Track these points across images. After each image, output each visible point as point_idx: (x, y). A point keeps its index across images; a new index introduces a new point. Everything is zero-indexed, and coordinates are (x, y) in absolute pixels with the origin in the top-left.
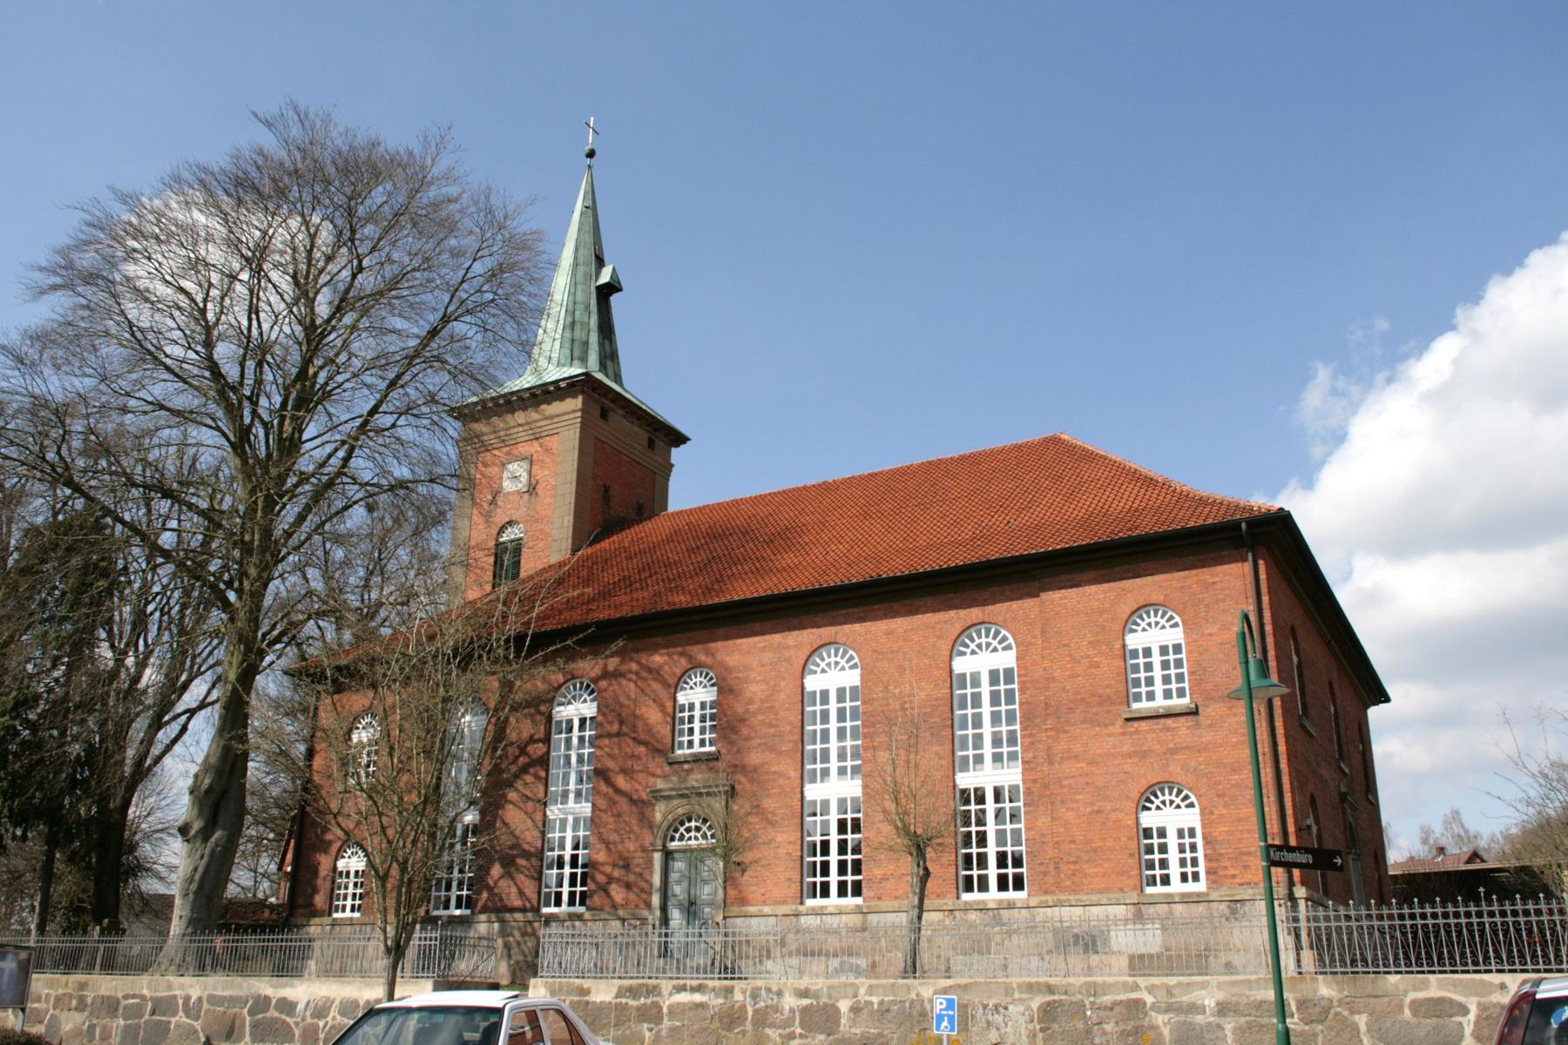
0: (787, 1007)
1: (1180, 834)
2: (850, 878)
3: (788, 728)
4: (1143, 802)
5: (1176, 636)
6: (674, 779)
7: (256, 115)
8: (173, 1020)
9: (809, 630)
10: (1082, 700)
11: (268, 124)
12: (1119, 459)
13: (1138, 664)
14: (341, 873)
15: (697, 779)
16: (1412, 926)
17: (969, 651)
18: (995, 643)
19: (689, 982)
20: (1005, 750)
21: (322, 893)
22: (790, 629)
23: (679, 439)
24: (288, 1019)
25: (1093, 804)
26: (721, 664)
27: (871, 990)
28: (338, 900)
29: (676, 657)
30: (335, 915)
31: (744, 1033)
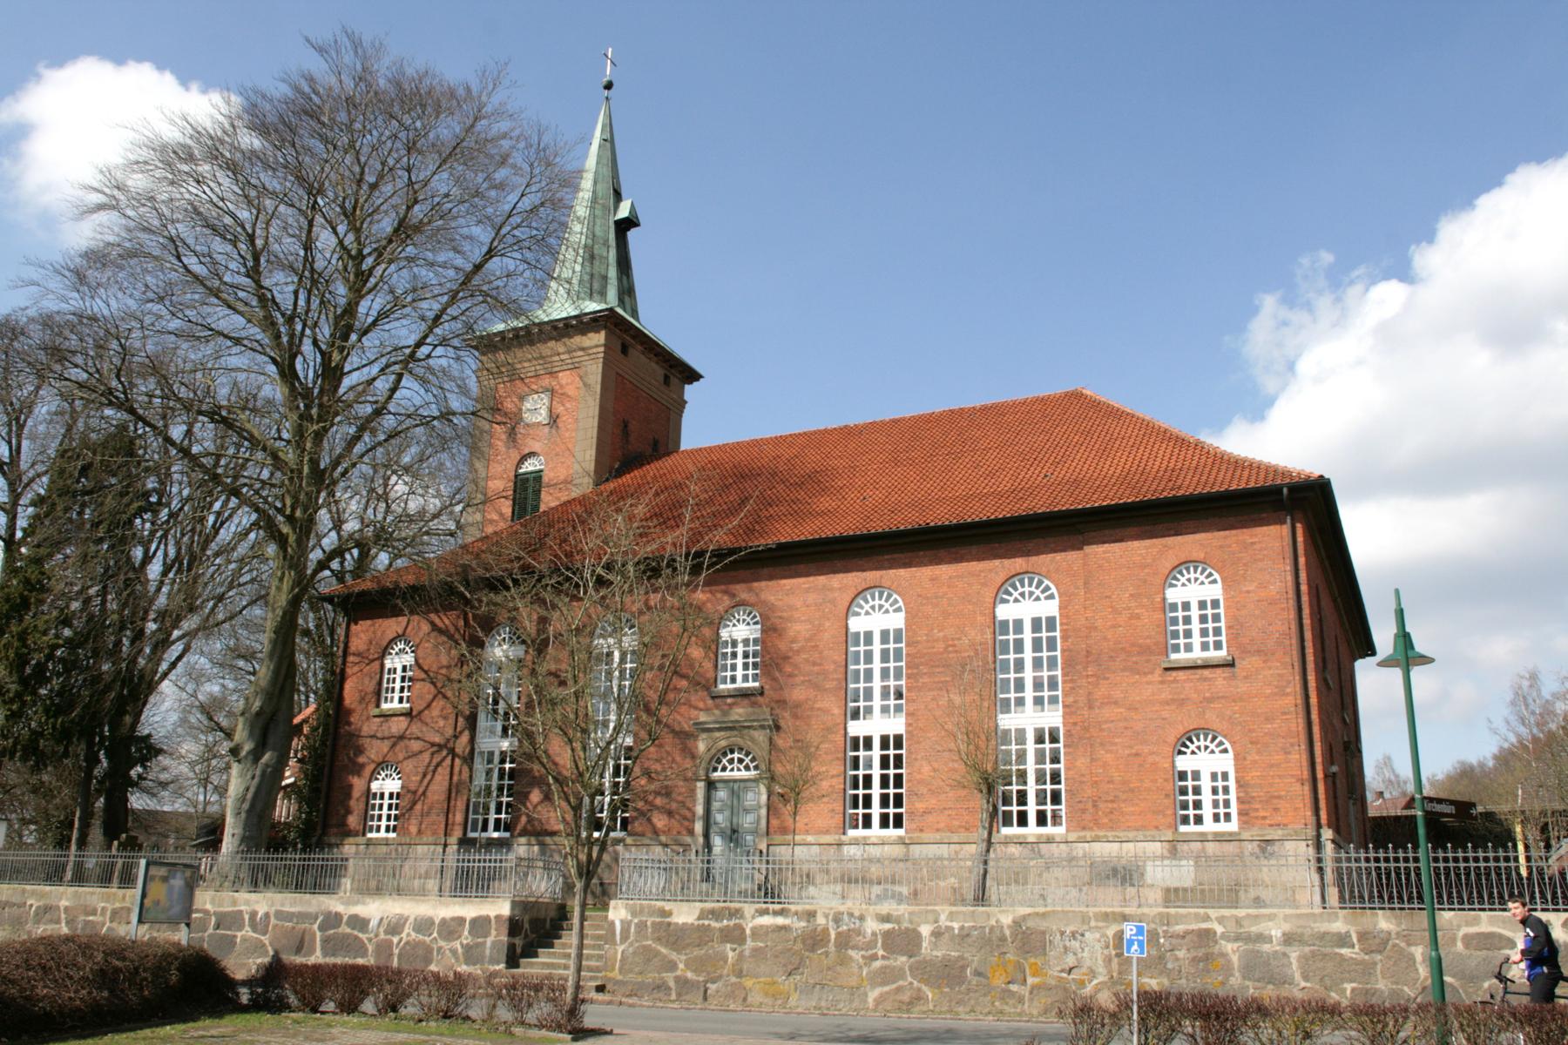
0: (869, 931)
1: (1214, 777)
2: (891, 811)
3: (832, 667)
4: (1179, 747)
5: (1215, 591)
6: (717, 712)
7: (308, 40)
8: (239, 934)
9: (854, 574)
10: (1122, 649)
11: (321, 50)
12: (1148, 418)
13: (1177, 618)
14: (375, 794)
15: (739, 713)
16: (1465, 868)
17: (1012, 599)
18: (1038, 592)
19: (771, 907)
20: (1046, 694)
21: (355, 813)
22: (835, 572)
23: (692, 376)
24: (361, 935)
25: (1131, 747)
26: (764, 603)
27: (951, 916)
28: (372, 820)
29: (719, 595)
30: (369, 835)
31: (827, 954)
